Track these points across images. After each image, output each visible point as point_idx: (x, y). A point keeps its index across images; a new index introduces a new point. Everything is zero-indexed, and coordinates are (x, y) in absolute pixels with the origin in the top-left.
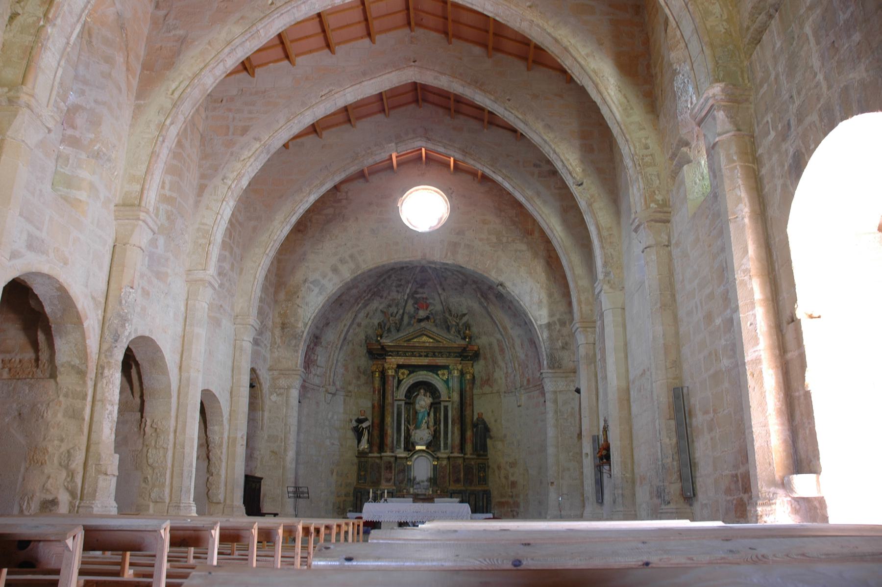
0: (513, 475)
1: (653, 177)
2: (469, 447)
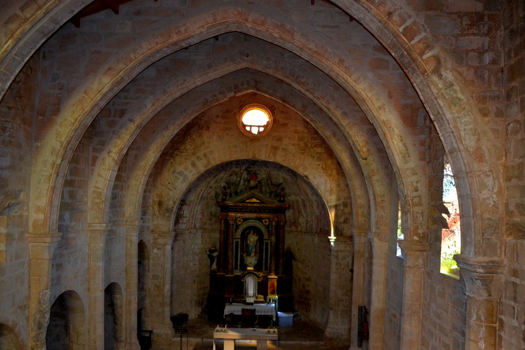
0: (308, 286)
1: (418, 215)
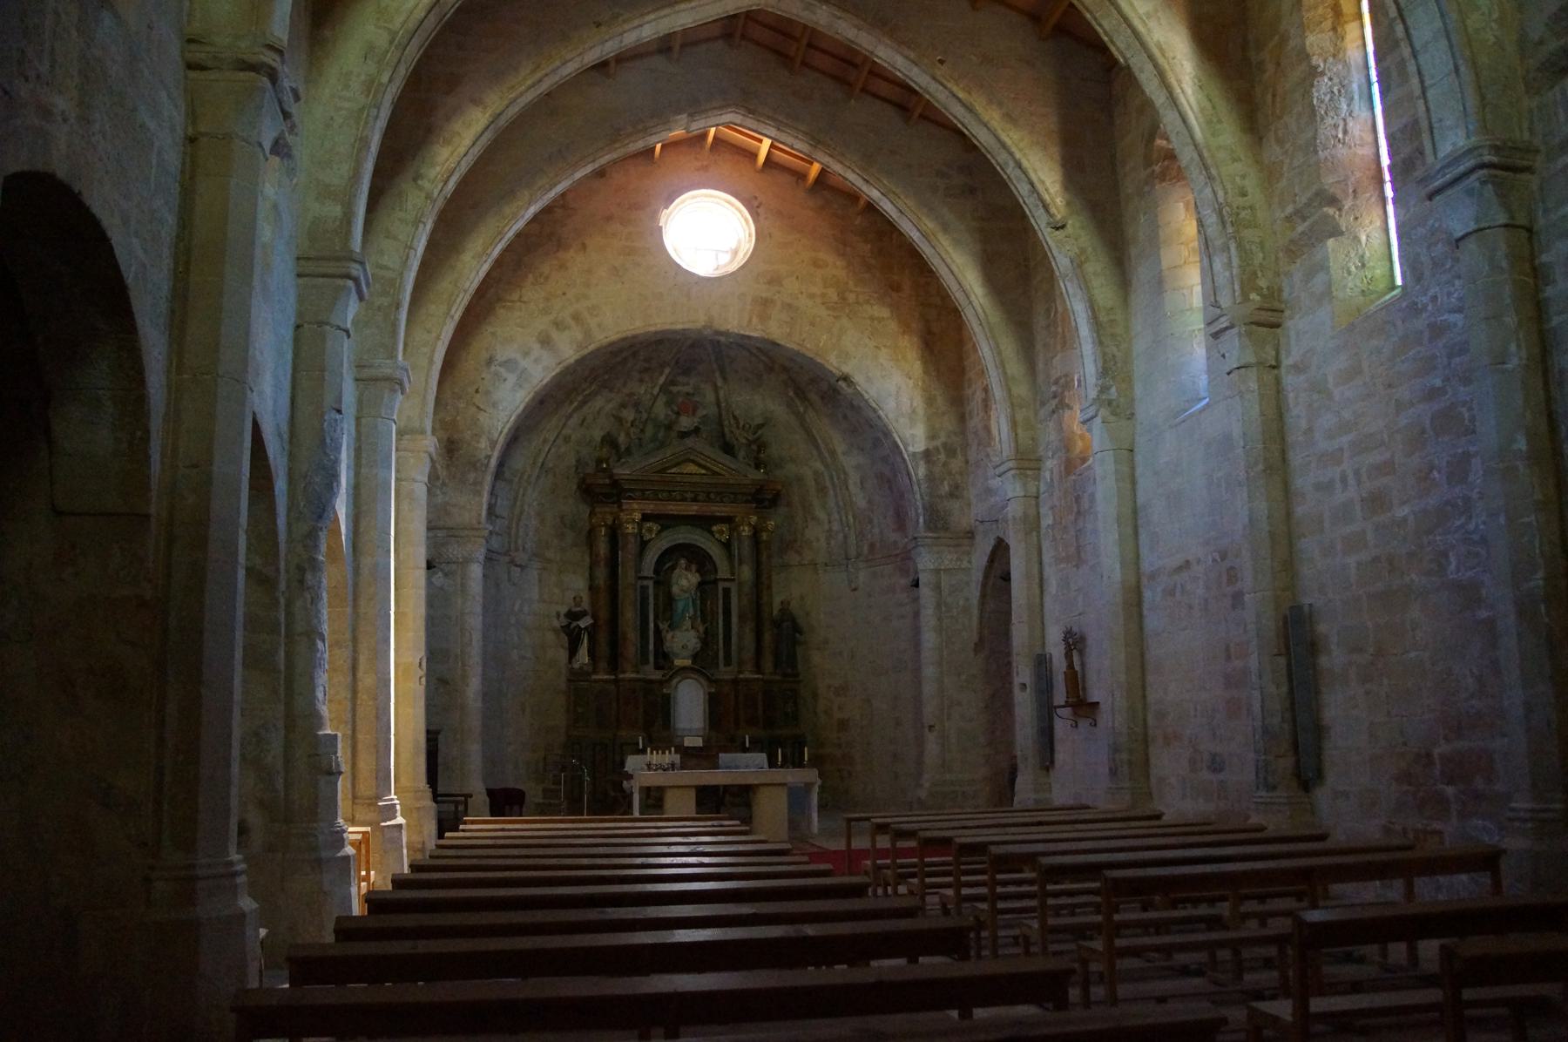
2: (768, 665)
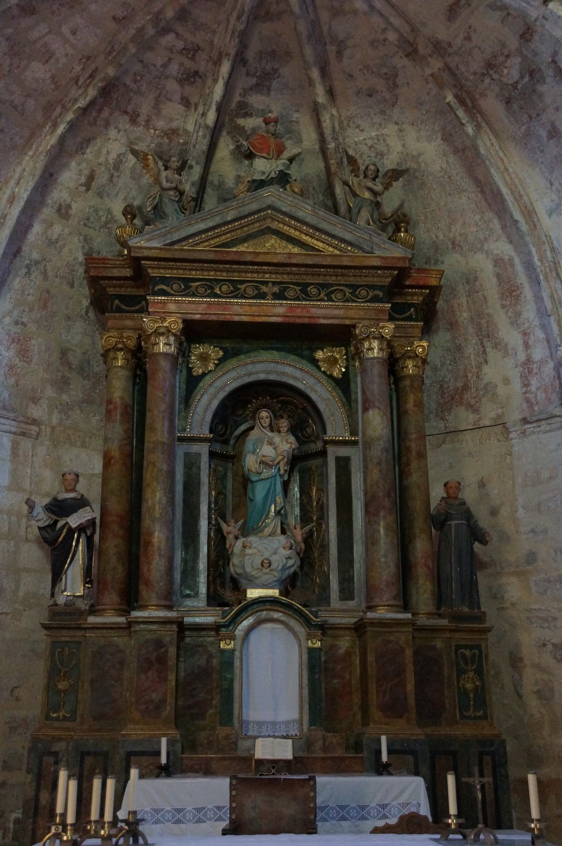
2: (423, 592)
